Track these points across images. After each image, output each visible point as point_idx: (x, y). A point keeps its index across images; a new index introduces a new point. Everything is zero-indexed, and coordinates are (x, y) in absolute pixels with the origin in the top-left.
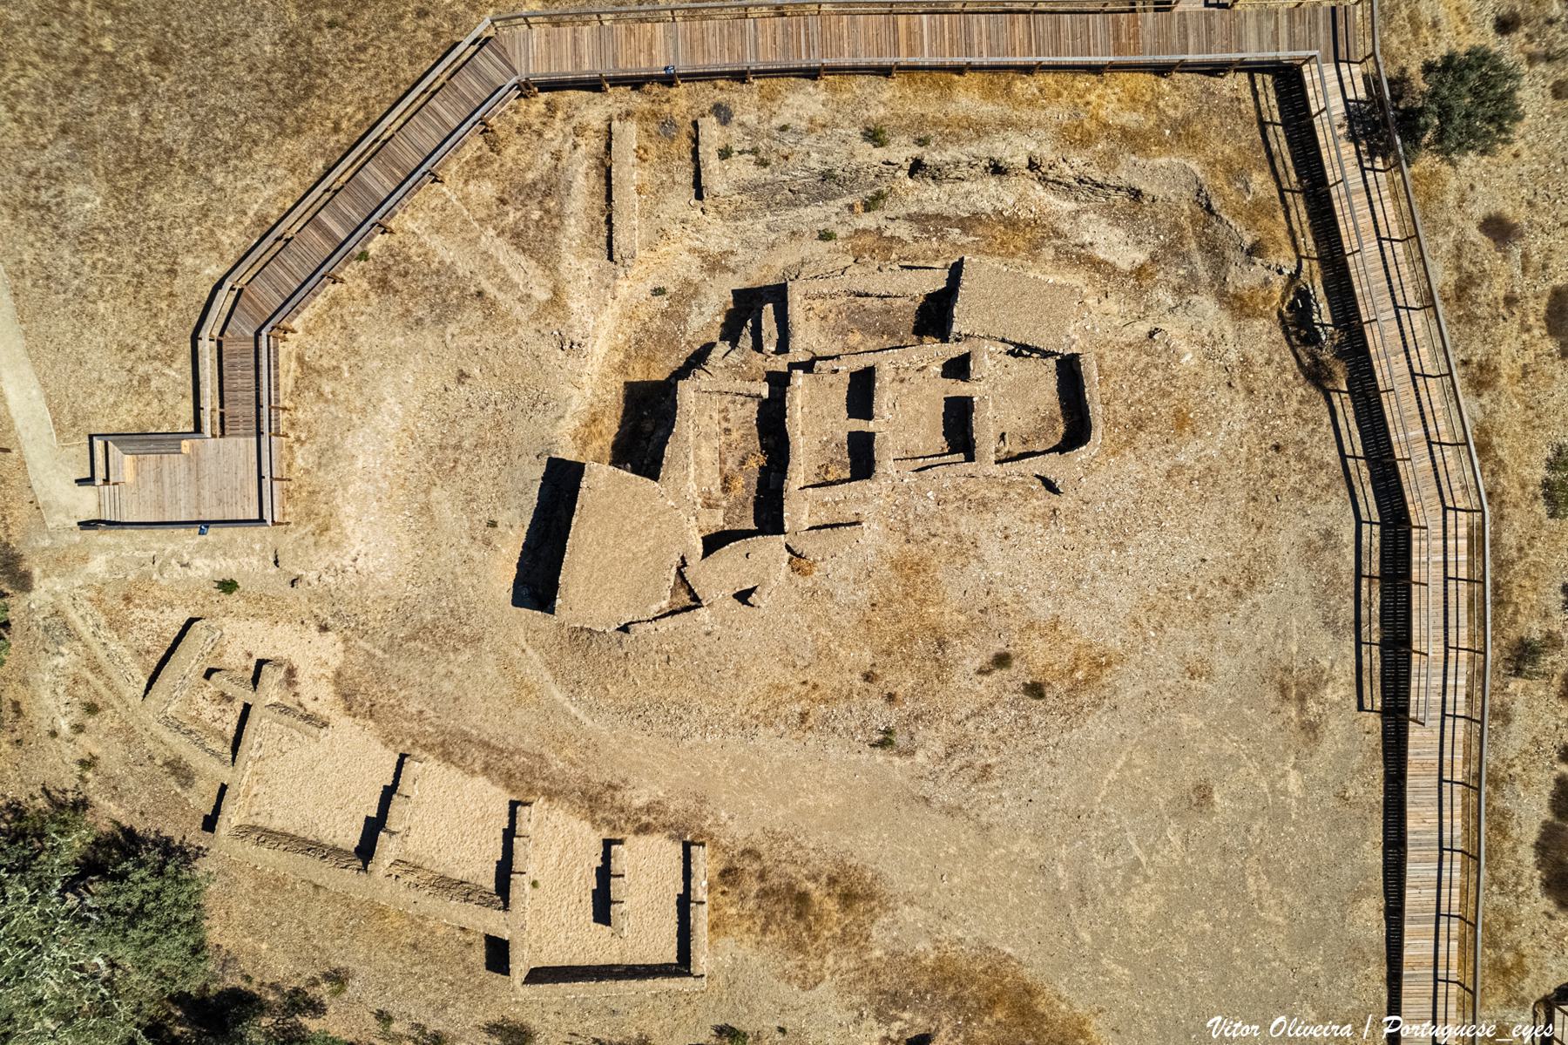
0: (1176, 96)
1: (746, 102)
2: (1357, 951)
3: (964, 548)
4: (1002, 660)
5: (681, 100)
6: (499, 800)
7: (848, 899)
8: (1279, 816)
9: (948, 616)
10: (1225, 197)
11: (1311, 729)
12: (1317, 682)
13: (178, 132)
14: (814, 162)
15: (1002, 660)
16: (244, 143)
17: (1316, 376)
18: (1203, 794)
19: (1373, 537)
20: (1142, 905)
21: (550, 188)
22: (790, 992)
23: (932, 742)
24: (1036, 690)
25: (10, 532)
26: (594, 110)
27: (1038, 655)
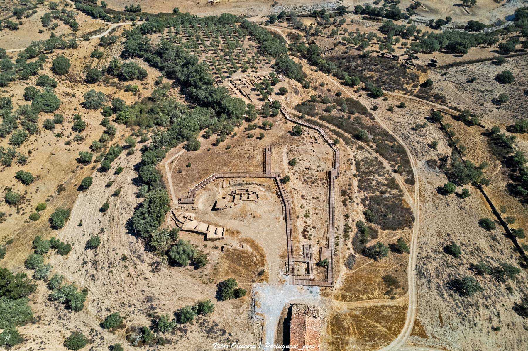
0: (267, 179)
1: (234, 179)
2: (284, 239)
3: (248, 205)
4: (251, 214)
5: (229, 179)
6: (207, 225)
7: (237, 233)
8: (276, 228)
9: (247, 210)
10: (271, 185)
11: (279, 222)
12: (279, 218)
13: (189, 181)
14: (341, 178)
15: (251, 214)
16: (195, 181)
17: (279, 197)
18: (269, 226)
19: (284, 208)
20: (264, 234)
21: (218, 184)
22: (232, 240)
23: (245, 221)
24: (254, 217)
25: (34, 250)
26: (222, 179)
27: (254, 214)
